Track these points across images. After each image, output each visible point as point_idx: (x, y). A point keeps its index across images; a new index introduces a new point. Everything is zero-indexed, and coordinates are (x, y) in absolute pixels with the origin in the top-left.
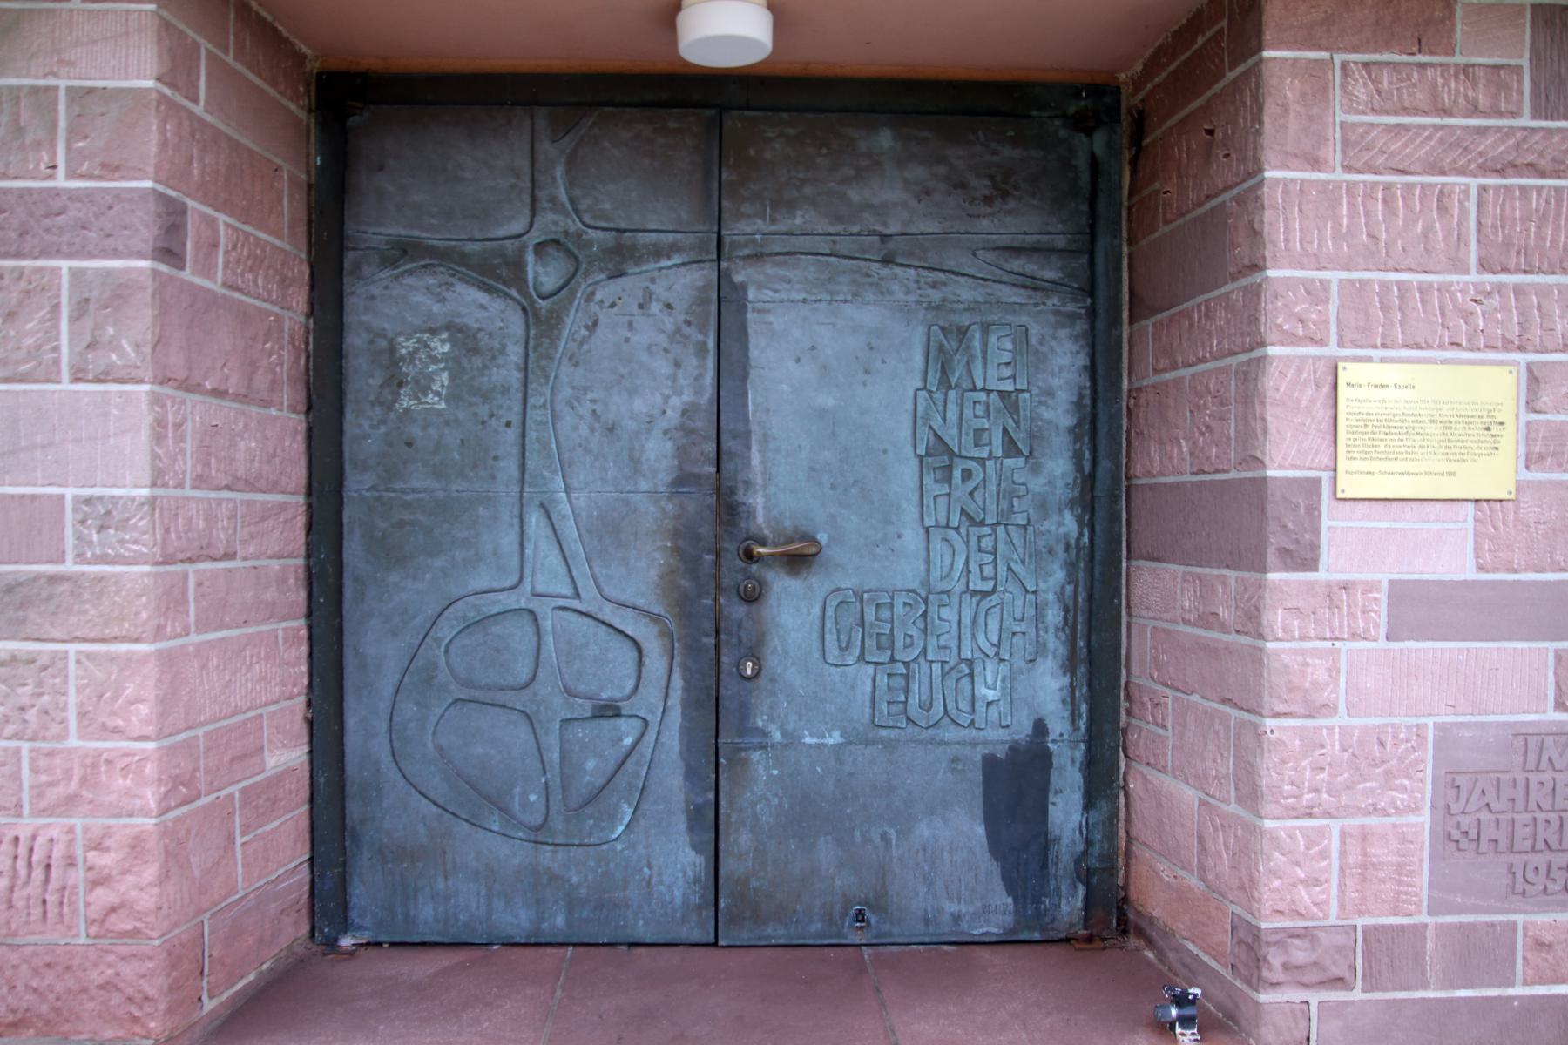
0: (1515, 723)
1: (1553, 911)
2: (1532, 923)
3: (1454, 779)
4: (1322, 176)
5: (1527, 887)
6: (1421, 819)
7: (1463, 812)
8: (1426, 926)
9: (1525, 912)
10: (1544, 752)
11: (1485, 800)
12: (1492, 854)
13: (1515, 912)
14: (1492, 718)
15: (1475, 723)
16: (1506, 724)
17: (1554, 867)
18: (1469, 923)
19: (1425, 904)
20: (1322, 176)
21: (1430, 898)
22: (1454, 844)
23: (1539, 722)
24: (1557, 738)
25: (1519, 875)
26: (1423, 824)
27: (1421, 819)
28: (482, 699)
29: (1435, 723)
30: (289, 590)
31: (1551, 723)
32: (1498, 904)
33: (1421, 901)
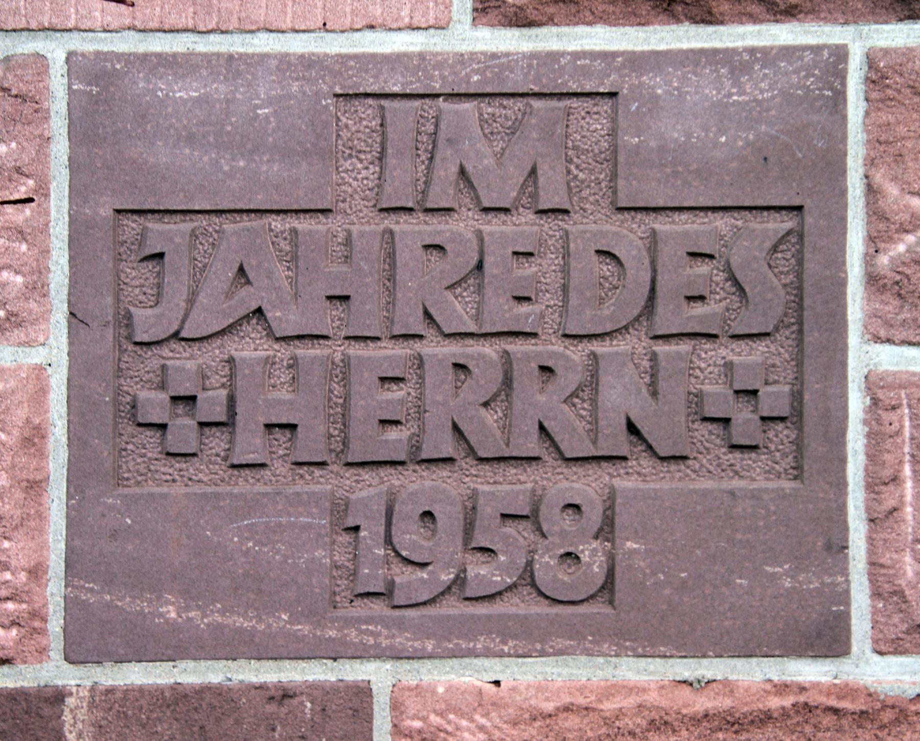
0: (343, 58)
1: (488, 653)
2: (418, 689)
3: (143, 234)
4: (540, 348)
5: (404, 576)
6: (37, 356)
7: (176, 336)
8: (58, 697)
9: (398, 656)
10: (444, 151)
11: (249, 298)
12: (281, 468)
13: (361, 654)
14: (263, 43)
15: (207, 57)
16: (309, 62)
17: (488, 511)
18: (204, 690)
19: (55, 625)
20: (540, 348)
21: (70, 604)
22: (150, 437)
23: (422, 56)
24: (488, 109)
25: (372, 532)
26: (39, 371)
27: (37, 356)
28: (191, 37)
29: (70, 56)
30: (698, 82)
31: (462, 59)
32: (303, 628)
33: (39, 615)
